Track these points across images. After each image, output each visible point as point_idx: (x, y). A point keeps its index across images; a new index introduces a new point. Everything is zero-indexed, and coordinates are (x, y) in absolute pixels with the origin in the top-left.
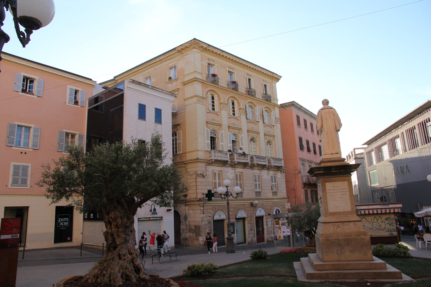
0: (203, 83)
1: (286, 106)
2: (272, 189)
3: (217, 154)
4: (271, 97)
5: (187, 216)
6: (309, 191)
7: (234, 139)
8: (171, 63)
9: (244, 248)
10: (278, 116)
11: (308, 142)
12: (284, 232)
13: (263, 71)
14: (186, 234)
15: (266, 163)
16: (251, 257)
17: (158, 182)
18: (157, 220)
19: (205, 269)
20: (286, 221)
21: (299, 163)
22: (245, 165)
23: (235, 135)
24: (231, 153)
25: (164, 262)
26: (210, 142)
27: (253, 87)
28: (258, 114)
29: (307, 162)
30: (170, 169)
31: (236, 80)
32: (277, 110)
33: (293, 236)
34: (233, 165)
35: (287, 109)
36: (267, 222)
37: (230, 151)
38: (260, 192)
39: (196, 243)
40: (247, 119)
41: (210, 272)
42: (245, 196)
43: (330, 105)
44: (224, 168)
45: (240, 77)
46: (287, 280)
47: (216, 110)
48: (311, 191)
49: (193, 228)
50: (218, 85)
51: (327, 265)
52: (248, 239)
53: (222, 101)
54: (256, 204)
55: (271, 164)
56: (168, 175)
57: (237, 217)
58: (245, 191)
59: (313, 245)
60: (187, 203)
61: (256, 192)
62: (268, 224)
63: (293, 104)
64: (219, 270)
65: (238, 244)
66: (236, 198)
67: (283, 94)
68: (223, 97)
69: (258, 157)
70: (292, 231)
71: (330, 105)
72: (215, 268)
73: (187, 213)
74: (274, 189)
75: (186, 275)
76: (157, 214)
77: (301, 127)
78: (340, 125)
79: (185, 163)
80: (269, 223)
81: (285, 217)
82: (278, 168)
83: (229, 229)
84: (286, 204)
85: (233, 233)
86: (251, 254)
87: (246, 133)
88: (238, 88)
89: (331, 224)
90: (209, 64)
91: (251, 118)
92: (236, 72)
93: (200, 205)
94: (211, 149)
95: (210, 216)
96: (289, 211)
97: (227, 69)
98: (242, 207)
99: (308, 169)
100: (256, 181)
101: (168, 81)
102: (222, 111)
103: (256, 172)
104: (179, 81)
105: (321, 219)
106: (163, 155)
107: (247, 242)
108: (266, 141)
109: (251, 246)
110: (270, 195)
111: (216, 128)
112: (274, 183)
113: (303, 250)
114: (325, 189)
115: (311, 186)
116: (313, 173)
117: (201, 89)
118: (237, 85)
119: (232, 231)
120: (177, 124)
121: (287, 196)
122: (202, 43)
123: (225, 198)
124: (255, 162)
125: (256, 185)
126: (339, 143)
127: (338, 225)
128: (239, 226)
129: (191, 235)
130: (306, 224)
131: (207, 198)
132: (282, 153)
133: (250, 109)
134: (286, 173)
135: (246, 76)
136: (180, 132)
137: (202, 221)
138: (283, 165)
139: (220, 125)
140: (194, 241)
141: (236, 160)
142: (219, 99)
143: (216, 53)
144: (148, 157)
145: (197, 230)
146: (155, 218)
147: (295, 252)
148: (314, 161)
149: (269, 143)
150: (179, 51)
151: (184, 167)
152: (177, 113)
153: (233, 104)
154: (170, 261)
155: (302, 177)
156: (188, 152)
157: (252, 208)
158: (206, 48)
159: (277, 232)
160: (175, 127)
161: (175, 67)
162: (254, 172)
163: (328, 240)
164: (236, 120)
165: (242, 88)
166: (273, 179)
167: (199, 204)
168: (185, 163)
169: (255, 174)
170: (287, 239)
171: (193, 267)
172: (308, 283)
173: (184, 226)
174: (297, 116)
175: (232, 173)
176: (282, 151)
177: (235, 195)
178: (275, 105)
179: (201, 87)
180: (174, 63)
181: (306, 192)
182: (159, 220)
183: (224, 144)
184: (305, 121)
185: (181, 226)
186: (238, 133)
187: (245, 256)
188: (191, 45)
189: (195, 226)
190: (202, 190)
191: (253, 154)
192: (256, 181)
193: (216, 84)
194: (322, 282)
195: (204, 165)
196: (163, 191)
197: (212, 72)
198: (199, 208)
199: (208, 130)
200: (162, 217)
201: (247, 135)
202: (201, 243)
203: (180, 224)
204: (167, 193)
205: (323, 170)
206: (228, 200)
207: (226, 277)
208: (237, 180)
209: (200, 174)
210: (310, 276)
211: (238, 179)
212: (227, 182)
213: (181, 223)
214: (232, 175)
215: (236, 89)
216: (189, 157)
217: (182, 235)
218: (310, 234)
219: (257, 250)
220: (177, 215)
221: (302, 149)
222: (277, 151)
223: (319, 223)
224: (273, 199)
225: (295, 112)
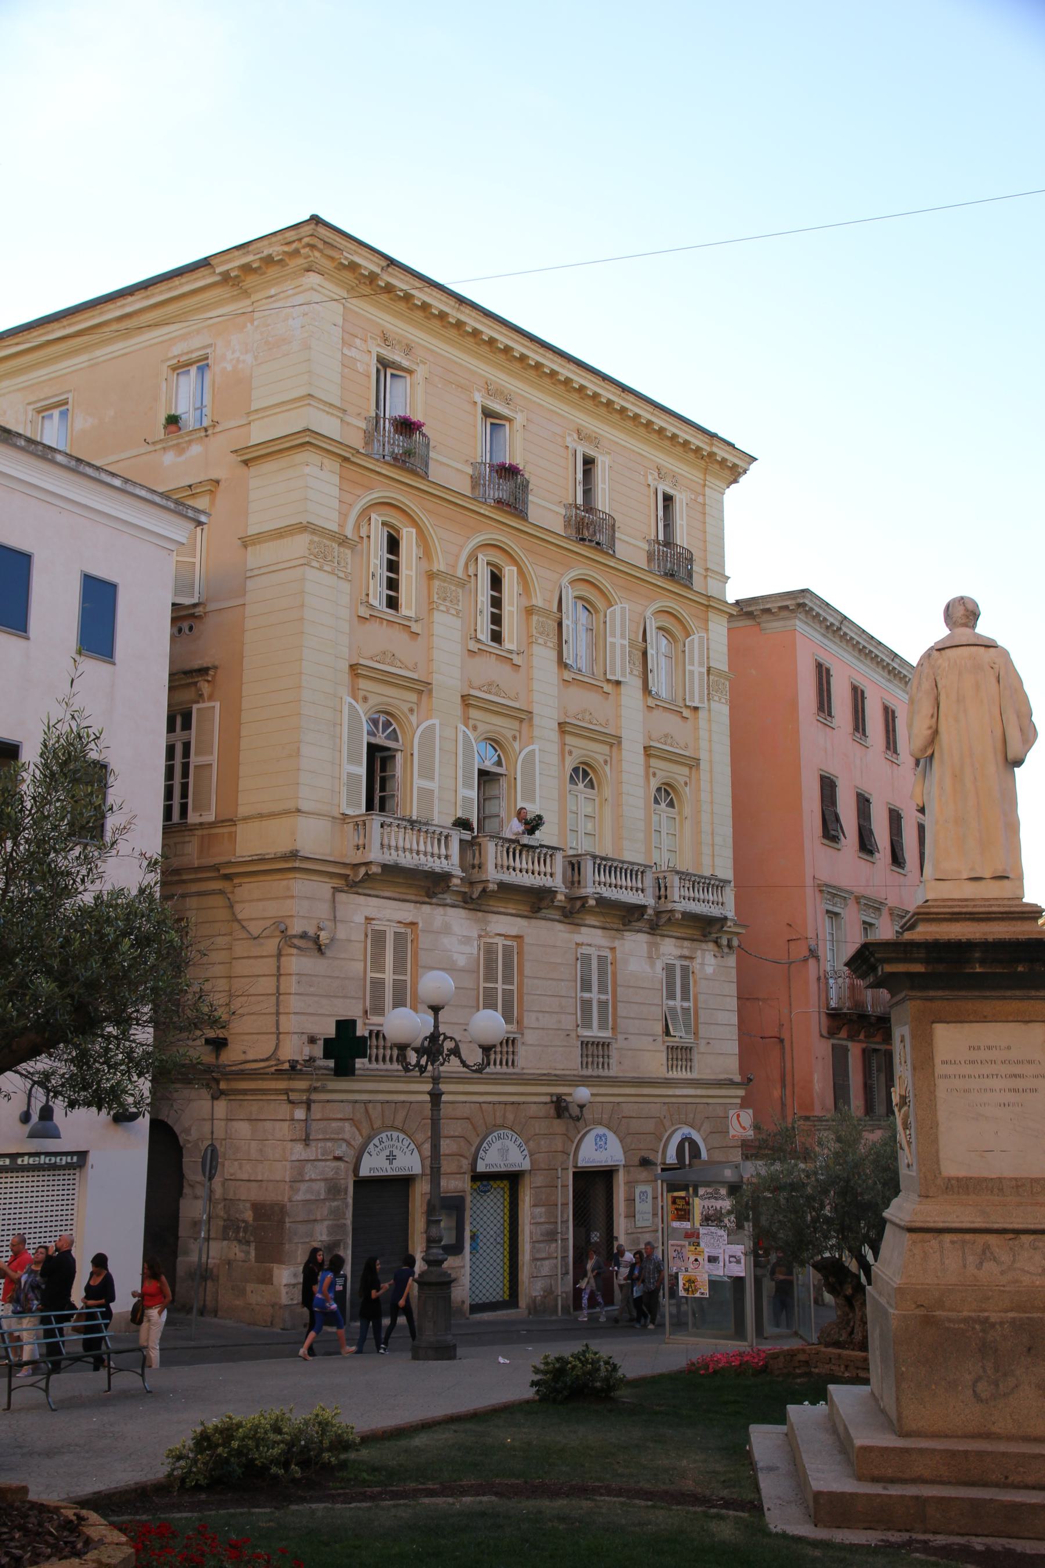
0: (346, 459)
1: (768, 611)
2: (667, 1033)
3: (399, 837)
4: (691, 560)
5: (221, 1149)
6: (855, 1051)
7: (489, 765)
8: (181, 339)
9: (506, 1336)
10: (721, 661)
11: (863, 803)
12: (713, 1259)
13: (660, 421)
14: (205, 1250)
15: (647, 899)
16: (533, 1384)
17: (62, 979)
18: (54, 1167)
19: (291, 1444)
20: (726, 1204)
21: (814, 907)
22: (536, 901)
23: (495, 742)
24: (467, 836)
25: (71, 1404)
26: (362, 771)
27: (603, 502)
28: (619, 641)
29: (852, 903)
30: (131, 913)
31: (518, 461)
32: (718, 630)
33: (758, 1281)
34: (478, 898)
35: (774, 626)
36: (630, 1201)
37: (463, 824)
38: (605, 1045)
39: (256, 1295)
40: (562, 664)
41: (313, 1464)
42: (526, 1060)
43: (984, 628)
44: (426, 908)
45: (543, 445)
46: (713, 1526)
47: (408, 608)
48: (867, 1055)
49: (249, 1216)
50: (425, 477)
51: (921, 1451)
52: (531, 1288)
53: (440, 565)
54: (581, 1107)
55: (670, 906)
56: (116, 944)
57: (481, 1167)
58: (530, 1037)
59: (858, 1337)
60: (223, 1085)
61: (585, 1044)
62: (637, 1215)
63: (801, 604)
64: (364, 1453)
65: (476, 1308)
66: (479, 1071)
67: (753, 562)
68: (447, 545)
69: (606, 865)
70: (756, 1256)
71: (984, 628)
72: (342, 1444)
73: (219, 1133)
74: (680, 1035)
75: (183, 1480)
76: (57, 1136)
77: (835, 723)
78: (1029, 735)
79: (228, 874)
80: (644, 1208)
81: (723, 1183)
82: (705, 928)
83: (434, 1231)
84: (731, 1113)
85: (456, 1249)
86: (537, 1371)
87: (555, 736)
88: (525, 503)
89: (947, 1238)
90: (384, 364)
91: (583, 664)
92: (520, 419)
93: (293, 1096)
94: (370, 807)
95: (338, 1159)
96: (751, 1150)
97: (478, 398)
98: (510, 1116)
99: (852, 941)
100: (586, 986)
101: (161, 433)
102: (437, 616)
103: (592, 938)
104: (221, 444)
105: (900, 1210)
106: (112, 822)
107: (523, 1302)
108: (654, 783)
109: (543, 1321)
110: (654, 1063)
111: (400, 700)
112: (678, 1003)
113: (807, 1363)
114: (931, 1058)
115: (859, 1029)
116: (873, 969)
117: (336, 492)
118: (525, 486)
119: (448, 1239)
120: (197, 664)
121: (742, 1070)
122: (353, 246)
123: (422, 1069)
124: (589, 889)
125: (586, 1004)
126: (1012, 827)
127: (987, 1247)
128: (485, 1215)
129: (236, 1251)
130: (822, 1222)
131: (331, 1063)
132: (729, 853)
133: (583, 615)
134: (744, 953)
135: (571, 441)
136: (210, 712)
137: (298, 1179)
138: (731, 914)
139: (422, 688)
140: (249, 1287)
141: (492, 874)
142: (427, 553)
143: (425, 307)
144: (16, 844)
145: (266, 1226)
146: (43, 1159)
147: (764, 1370)
148: (891, 902)
149: (666, 794)
150: (226, 278)
151: (221, 892)
152: (198, 611)
153: (496, 582)
154: (107, 1399)
155: (822, 979)
156: (245, 819)
157: (558, 1126)
158: (373, 277)
159: (680, 1256)
160: (188, 681)
161: (202, 364)
162: (578, 938)
163: (927, 1321)
164: (507, 668)
165: (549, 503)
166: (679, 981)
167: (286, 1092)
168: (228, 874)
169: (585, 950)
170: (728, 1295)
171: (227, 1432)
172: (816, 1544)
173: (200, 1204)
174: (819, 666)
175: (466, 940)
176: (730, 841)
177: (474, 1057)
178: (712, 604)
179: (336, 479)
180: (197, 342)
181: (839, 1056)
182: (69, 1166)
183: (438, 784)
184: (858, 696)
185: (183, 1203)
186: (509, 734)
187: (500, 1377)
188: (296, 253)
189: (258, 1208)
190: (307, 1019)
191: (584, 846)
192: (586, 986)
193: (413, 472)
194: (889, 1545)
195: (323, 888)
196: (87, 1023)
197: (397, 407)
198: (284, 1110)
199: (360, 708)
200: (83, 1155)
201: (555, 748)
202: (285, 1300)
203: (180, 1193)
204: (108, 1038)
205: (927, 961)
206: (436, 1080)
207: (395, 1495)
208: (490, 976)
209: (304, 936)
210: (829, 1508)
211: (500, 969)
212: (435, 983)
213: (186, 1190)
214: (467, 949)
215: (514, 505)
216: (250, 842)
217: (186, 1253)
218: (847, 1285)
219: (567, 1349)
220: (165, 1145)
221: (835, 839)
222: (703, 841)
223: (889, 1230)
224: (667, 1083)
225: (809, 644)
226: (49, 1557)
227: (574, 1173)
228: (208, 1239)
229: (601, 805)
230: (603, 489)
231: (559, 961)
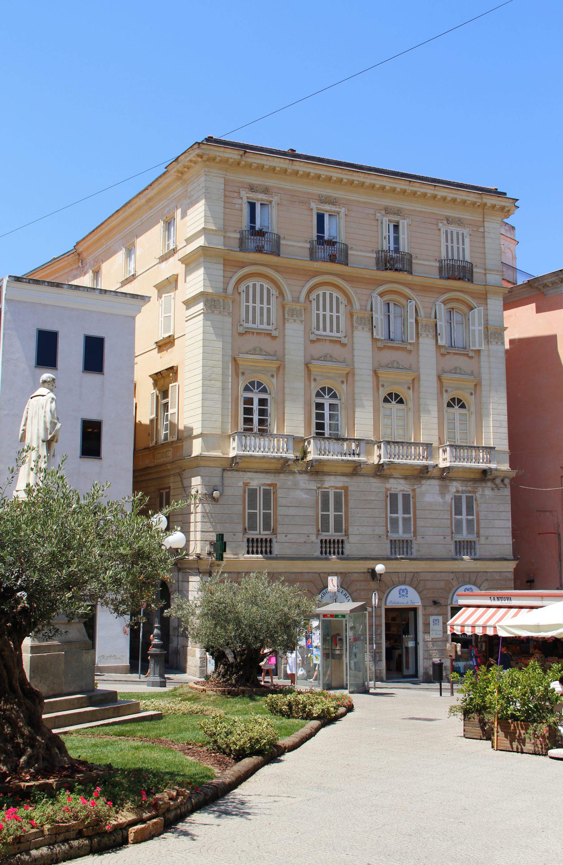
58: (352, 539)
102: (287, 325)
164: (338, 346)
226: (152, 772)
227: (386, 609)
228: (178, 636)
229: (407, 412)
230: (404, 238)
231: (373, 498)
